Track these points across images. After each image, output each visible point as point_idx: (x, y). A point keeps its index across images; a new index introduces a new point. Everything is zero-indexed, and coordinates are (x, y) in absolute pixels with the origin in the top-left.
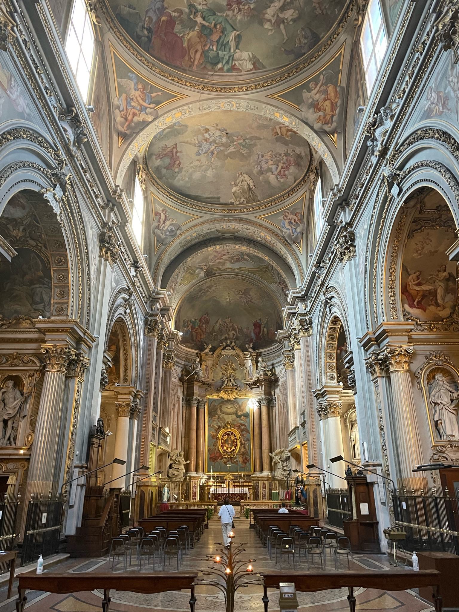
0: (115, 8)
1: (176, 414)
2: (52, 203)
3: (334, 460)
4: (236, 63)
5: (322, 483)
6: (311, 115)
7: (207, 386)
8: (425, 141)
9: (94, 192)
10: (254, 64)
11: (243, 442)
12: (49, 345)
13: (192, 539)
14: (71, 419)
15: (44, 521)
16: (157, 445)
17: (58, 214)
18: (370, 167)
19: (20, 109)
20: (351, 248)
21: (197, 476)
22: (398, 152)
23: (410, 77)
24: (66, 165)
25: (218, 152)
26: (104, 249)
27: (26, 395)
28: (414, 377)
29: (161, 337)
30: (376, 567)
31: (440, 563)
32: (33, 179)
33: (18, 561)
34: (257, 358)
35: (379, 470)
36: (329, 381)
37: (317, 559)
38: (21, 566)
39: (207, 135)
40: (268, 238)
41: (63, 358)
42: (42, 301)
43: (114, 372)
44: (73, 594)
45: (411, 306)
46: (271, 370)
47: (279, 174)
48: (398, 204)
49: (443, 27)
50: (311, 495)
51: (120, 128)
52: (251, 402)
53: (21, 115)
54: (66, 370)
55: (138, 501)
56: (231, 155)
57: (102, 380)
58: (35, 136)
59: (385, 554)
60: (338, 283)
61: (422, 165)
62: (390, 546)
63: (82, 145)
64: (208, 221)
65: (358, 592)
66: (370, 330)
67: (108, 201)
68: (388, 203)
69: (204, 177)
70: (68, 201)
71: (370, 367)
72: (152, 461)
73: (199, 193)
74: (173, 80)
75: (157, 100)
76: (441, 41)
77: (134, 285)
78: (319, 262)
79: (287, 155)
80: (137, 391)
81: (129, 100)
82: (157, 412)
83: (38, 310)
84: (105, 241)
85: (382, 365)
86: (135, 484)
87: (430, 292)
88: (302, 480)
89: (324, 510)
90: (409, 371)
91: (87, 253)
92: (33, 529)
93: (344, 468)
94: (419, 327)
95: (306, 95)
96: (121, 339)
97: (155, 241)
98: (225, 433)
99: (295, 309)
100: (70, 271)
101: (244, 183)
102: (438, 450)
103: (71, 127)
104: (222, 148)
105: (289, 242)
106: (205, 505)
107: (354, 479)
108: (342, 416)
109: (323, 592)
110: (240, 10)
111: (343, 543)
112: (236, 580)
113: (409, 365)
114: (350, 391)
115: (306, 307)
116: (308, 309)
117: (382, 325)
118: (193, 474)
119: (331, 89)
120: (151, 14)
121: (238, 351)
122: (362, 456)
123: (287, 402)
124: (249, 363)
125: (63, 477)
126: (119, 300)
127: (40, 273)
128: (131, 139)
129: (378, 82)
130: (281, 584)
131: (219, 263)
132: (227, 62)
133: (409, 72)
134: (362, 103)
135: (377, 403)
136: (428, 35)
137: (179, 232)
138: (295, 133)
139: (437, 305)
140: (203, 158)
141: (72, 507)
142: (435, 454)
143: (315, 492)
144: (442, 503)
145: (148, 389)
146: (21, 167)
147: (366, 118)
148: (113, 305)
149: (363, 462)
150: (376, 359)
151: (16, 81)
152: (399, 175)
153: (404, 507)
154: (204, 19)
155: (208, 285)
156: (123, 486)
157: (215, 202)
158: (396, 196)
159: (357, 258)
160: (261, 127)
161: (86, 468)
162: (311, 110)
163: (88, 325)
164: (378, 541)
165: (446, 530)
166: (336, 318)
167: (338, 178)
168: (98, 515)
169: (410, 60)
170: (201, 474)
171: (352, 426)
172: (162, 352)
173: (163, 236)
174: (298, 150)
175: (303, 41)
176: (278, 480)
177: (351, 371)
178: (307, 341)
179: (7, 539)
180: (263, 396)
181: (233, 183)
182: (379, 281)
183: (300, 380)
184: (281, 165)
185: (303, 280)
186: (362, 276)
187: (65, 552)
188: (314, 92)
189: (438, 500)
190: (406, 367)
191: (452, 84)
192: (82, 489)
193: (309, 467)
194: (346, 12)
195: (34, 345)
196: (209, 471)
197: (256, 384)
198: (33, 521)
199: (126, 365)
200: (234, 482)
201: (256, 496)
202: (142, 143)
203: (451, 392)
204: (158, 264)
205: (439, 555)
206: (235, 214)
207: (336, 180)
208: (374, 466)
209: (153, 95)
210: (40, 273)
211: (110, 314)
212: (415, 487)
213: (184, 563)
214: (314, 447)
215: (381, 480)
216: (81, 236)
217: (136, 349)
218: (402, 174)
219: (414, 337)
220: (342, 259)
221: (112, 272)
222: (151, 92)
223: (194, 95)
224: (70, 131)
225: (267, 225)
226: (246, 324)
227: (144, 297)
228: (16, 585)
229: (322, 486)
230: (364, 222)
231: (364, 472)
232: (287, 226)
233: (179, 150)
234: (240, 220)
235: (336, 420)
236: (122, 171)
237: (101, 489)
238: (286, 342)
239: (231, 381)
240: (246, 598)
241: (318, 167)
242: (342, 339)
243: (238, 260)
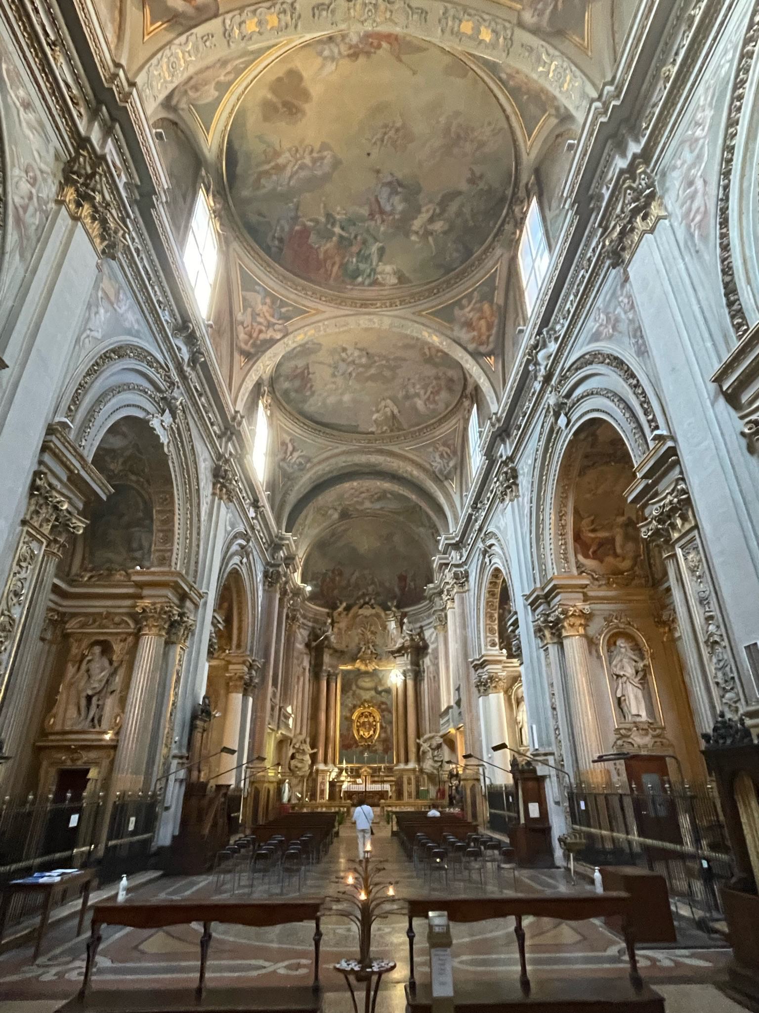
0: (243, 216)
1: (300, 689)
2: (159, 431)
3: (496, 749)
4: (379, 276)
5: (482, 778)
6: (464, 335)
7: (341, 655)
8: (594, 366)
9: (210, 419)
10: (399, 278)
11: (384, 725)
12: (147, 602)
13: (318, 852)
14: (169, 695)
15: (131, 827)
16: (276, 729)
17: (166, 443)
18: (534, 394)
19: (127, 325)
20: (514, 487)
21: (326, 768)
22: (564, 378)
23: (576, 296)
24: (178, 387)
25: (358, 374)
26: (219, 485)
27: (115, 664)
28: (591, 643)
29: (284, 593)
30: (549, 886)
31: (630, 882)
32: (135, 403)
33: (95, 883)
34: (402, 620)
35: (551, 759)
36: (489, 647)
37: (475, 876)
38: (99, 888)
39: (344, 355)
40: (415, 473)
41: (163, 619)
42: (141, 548)
43: (225, 636)
44: (164, 928)
45: (586, 556)
46: (419, 634)
47: (428, 399)
48: (566, 437)
49: (611, 242)
50: (468, 792)
51: (243, 346)
52: (395, 675)
53: (129, 332)
54: (167, 633)
55: (250, 801)
56: (372, 378)
57: (211, 645)
58: (142, 355)
59: (558, 868)
60: (498, 528)
61: (592, 394)
62: (567, 858)
63: (198, 366)
64: (343, 453)
65: (527, 921)
66: (538, 585)
67: (226, 429)
68: (554, 435)
69: (340, 402)
70: (178, 429)
71: (539, 630)
72: (270, 750)
73: (333, 421)
74: (306, 294)
75: (286, 314)
76: (609, 258)
77: (252, 528)
78: (475, 503)
79: (437, 378)
80: (253, 661)
81: (255, 315)
82: (276, 687)
83: (135, 559)
84: (220, 476)
85: (552, 630)
86: (247, 780)
87: (606, 539)
88: (457, 773)
89: (485, 811)
90: (586, 636)
91: (198, 490)
92: (117, 838)
93: (509, 758)
94: (596, 583)
95: (457, 312)
96: (235, 596)
97: (281, 480)
98: (362, 714)
99: (447, 559)
100: (177, 511)
101: (387, 409)
102: (622, 735)
103: (186, 344)
104: (361, 369)
105: (440, 479)
106: (335, 807)
107: (522, 772)
108: (506, 692)
109: (483, 923)
110: (383, 221)
111: (508, 856)
112: (373, 911)
113: (585, 629)
114: (515, 660)
115: (461, 556)
116: (464, 559)
117: (552, 579)
118: (321, 766)
119: (486, 306)
120: (283, 222)
121: (378, 610)
122: (530, 741)
123: (438, 674)
124: (392, 625)
125: (157, 770)
126: (234, 548)
127: (141, 514)
128: (255, 359)
129: (539, 301)
130: (431, 914)
131: (357, 501)
132: (369, 276)
133: (574, 291)
134: (522, 323)
135: (548, 677)
136: (594, 251)
137: (308, 465)
138: (446, 354)
139: (616, 555)
140: (339, 380)
141: (167, 809)
142: (618, 739)
143: (473, 788)
144: (628, 802)
145: (266, 656)
146: (124, 390)
147: (527, 340)
148: (227, 552)
149: (531, 750)
150: (546, 621)
151: (125, 293)
152: (566, 404)
153: (583, 807)
154: (343, 228)
155: (342, 528)
156: (232, 782)
157: (353, 430)
158: (563, 427)
159: (520, 499)
160: (407, 347)
161: (187, 758)
162: (464, 330)
163: (195, 577)
164: (550, 852)
165: (635, 837)
166: (497, 570)
167: (497, 407)
168: (200, 819)
169: (575, 277)
170: (330, 766)
171: (518, 704)
172: (285, 611)
173: (290, 470)
174: (450, 373)
175: (455, 255)
176: (427, 774)
177: (515, 636)
178: (463, 598)
179: (83, 852)
180: (409, 667)
181: (374, 409)
182: (548, 527)
183: (454, 646)
184: (430, 390)
185: (457, 523)
186: (526, 520)
187: (155, 868)
188: (467, 310)
189: (624, 797)
190: (581, 631)
191: (622, 304)
192: (180, 785)
193: (465, 757)
194: (502, 225)
195: (128, 602)
196: (341, 762)
197: (401, 651)
198: (118, 829)
199: (240, 629)
200: (372, 776)
201: (399, 794)
202: (268, 363)
203: (636, 661)
204: (283, 503)
205: (629, 870)
206: (378, 445)
207: (494, 408)
208: (546, 755)
209: (283, 310)
210: (141, 514)
211: (222, 565)
212: (595, 780)
213: (309, 882)
214: (471, 730)
215: (553, 772)
216: (192, 470)
217: (254, 615)
218: (569, 402)
219: (591, 594)
220: (503, 500)
221: (227, 513)
222: (281, 307)
223: (329, 310)
224: (184, 349)
225: (415, 458)
226: (388, 577)
227: (264, 544)
228: (89, 916)
229: (482, 781)
230: (528, 457)
231: (534, 763)
232: (438, 459)
233: (311, 370)
234: (381, 452)
235: (498, 698)
236: (244, 395)
237: (204, 785)
238: (437, 599)
239: (369, 648)
240: (387, 930)
241: (474, 393)
242: (505, 597)
243: (379, 499)
